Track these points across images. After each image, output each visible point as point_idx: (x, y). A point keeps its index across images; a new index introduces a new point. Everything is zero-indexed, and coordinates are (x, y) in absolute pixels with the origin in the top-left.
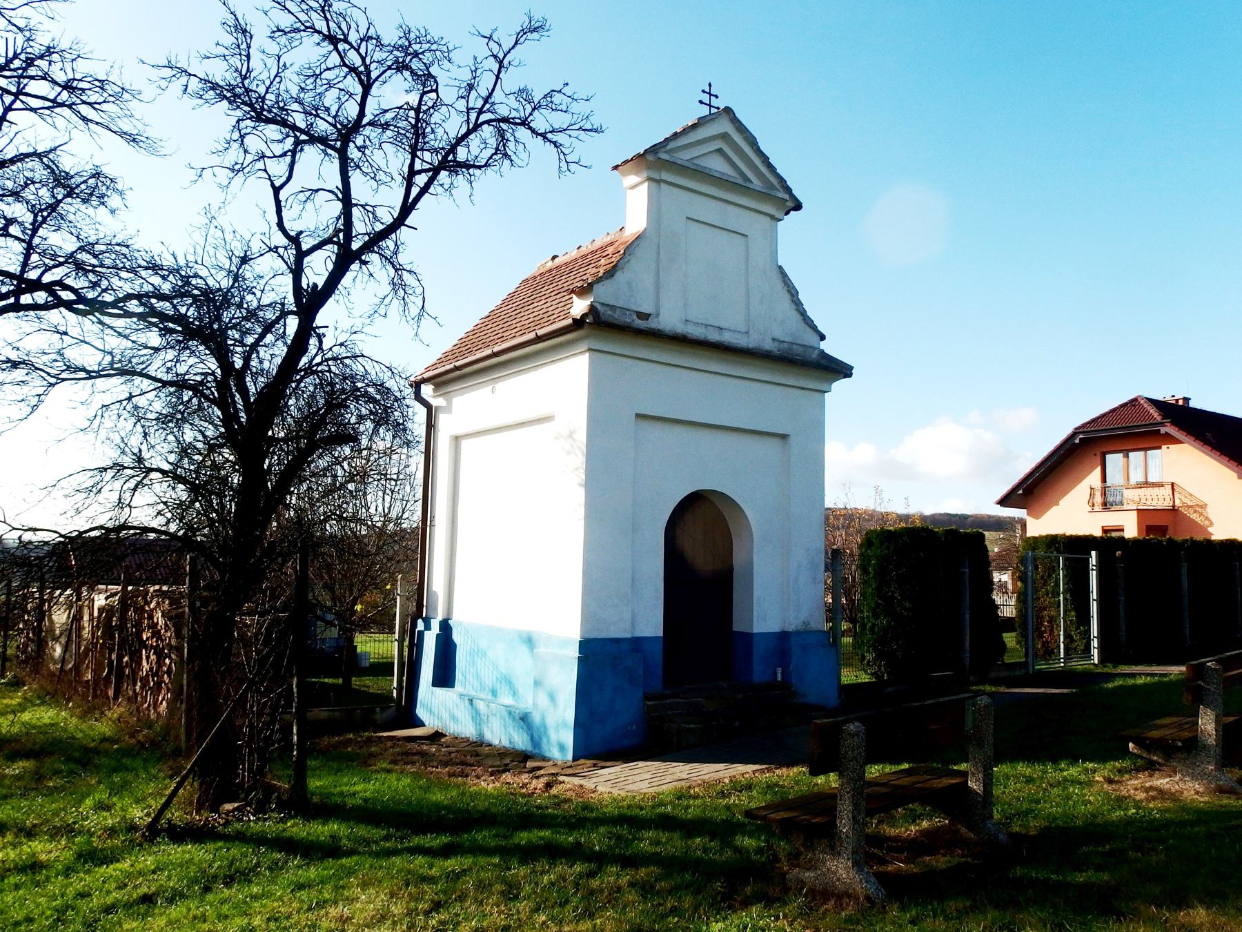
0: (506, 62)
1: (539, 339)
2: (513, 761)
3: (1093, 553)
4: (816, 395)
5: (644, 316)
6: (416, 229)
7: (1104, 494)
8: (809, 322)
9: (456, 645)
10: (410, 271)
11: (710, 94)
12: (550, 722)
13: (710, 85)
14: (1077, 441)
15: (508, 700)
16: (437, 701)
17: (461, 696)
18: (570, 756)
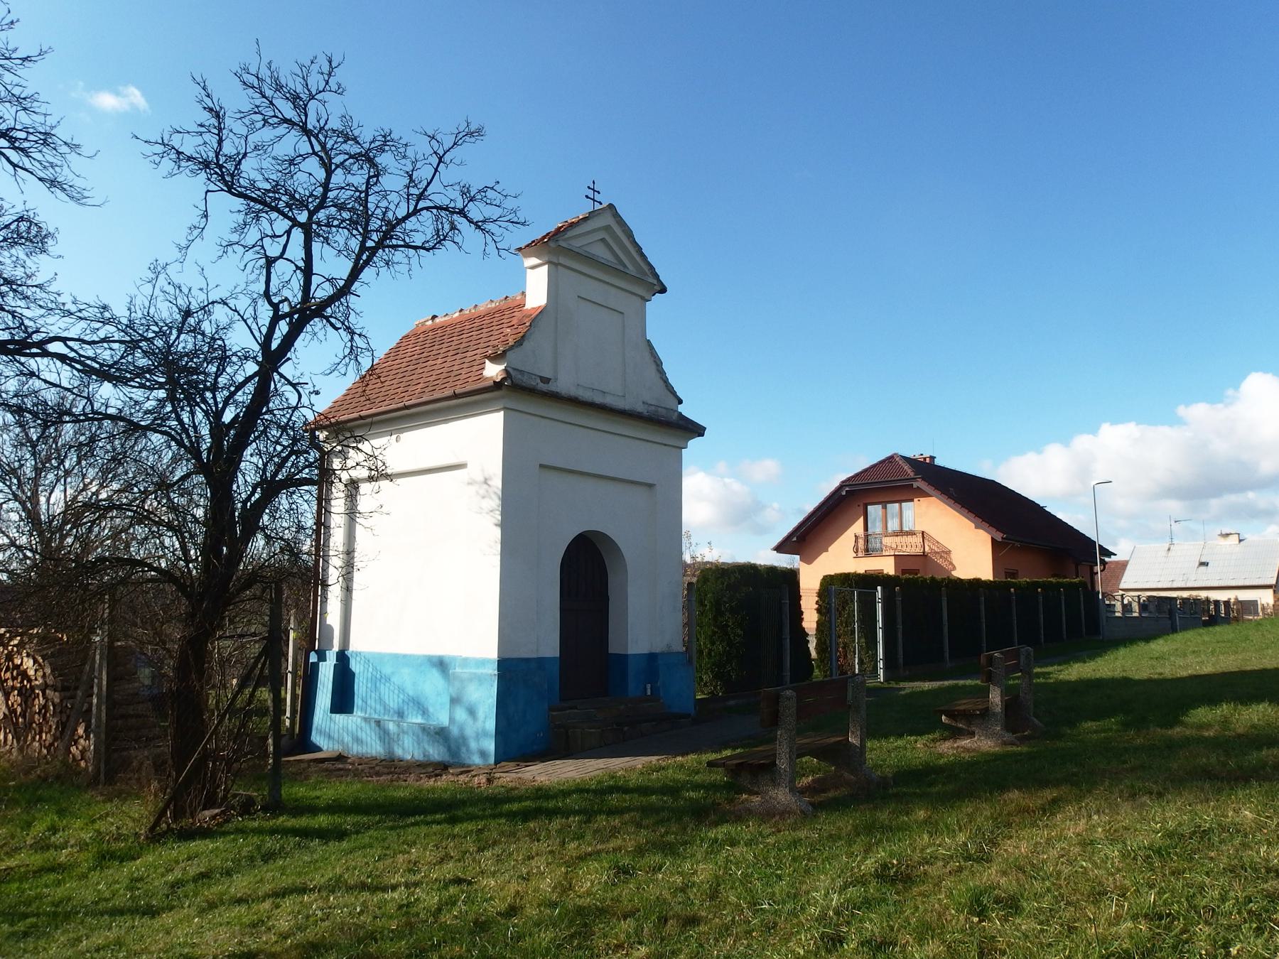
0: (447, 158)
1: (456, 396)
3: (879, 588)
4: (678, 450)
5: (546, 380)
7: (867, 541)
9: (353, 674)
10: (360, 335)
11: (593, 189)
12: (469, 732)
13: (594, 182)
14: (844, 493)
16: (337, 727)
18: (492, 760)
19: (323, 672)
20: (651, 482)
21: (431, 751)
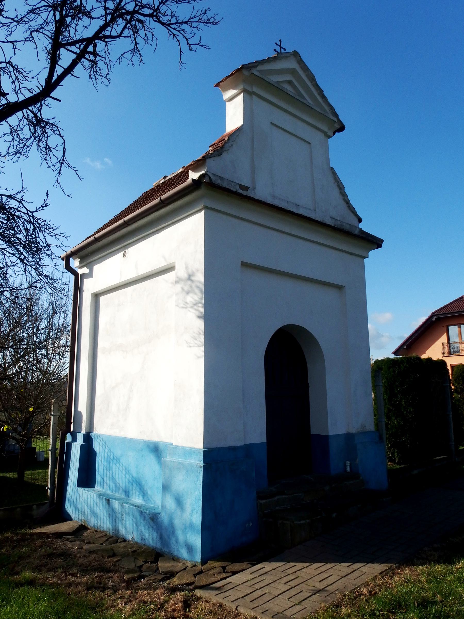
2: (146, 562)
4: (360, 259)
6: (60, 101)
7: (449, 347)
8: (352, 208)
9: (95, 454)
11: (280, 46)
12: (178, 523)
14: (434, 320)
15: (138, 500)
17: (100, 495)
18: (198, 558)
19: (74, 451)
20: (340, 283)
21: (147, 535)
